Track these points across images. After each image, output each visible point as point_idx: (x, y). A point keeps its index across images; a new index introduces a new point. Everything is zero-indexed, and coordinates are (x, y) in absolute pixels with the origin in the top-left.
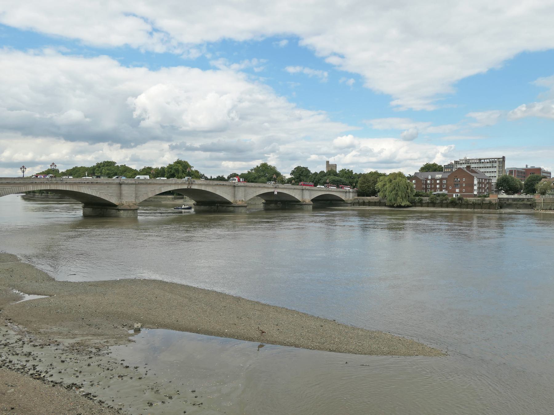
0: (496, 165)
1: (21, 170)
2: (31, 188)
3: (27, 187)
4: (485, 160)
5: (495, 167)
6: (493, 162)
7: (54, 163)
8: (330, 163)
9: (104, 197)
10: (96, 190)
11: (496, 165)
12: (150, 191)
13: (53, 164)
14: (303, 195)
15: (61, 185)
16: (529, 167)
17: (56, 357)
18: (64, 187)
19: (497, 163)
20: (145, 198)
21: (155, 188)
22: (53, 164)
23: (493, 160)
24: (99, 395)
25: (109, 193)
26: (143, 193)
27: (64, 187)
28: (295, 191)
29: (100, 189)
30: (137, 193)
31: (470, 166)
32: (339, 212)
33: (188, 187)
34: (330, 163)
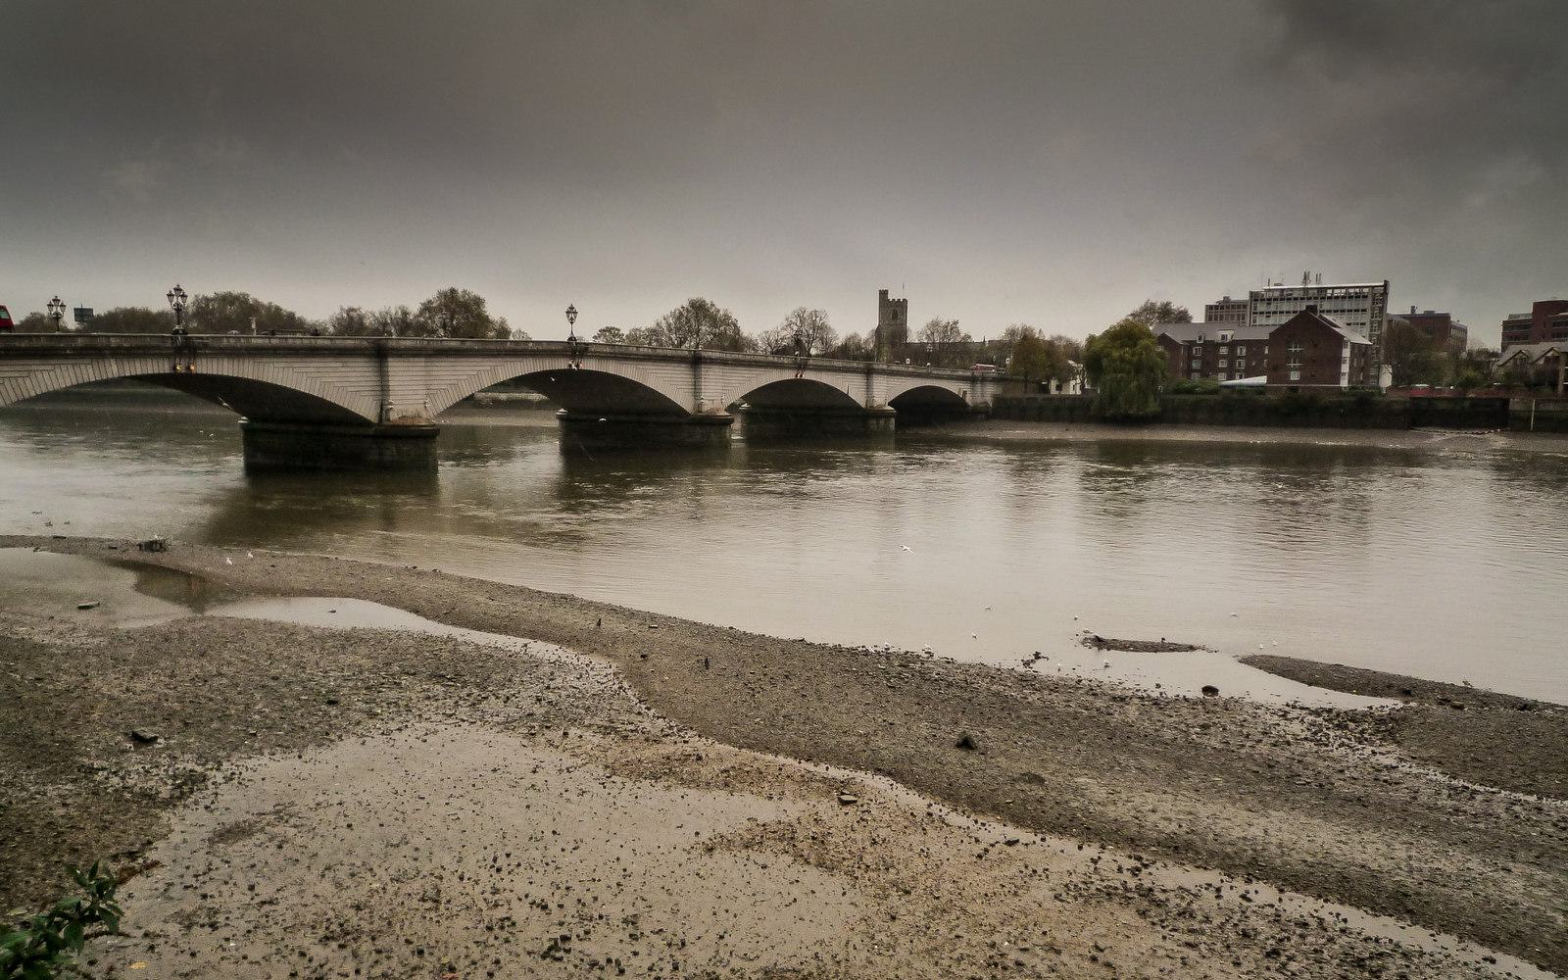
0: (1367, 304)
1: (171, 302)
2: (114, 368)
3: (261, 368)
4: (1336, 291)
5: (1364, 310)
6: (1357, 296)
7: (181, 287)
8: (890, 297)
9: (61, 380)
10: (313, 375)
11: (1367, 304)
12: (476, 373)
13: (56, 300)
14: (869, 387)
15: (204, 361)
16: (1419, 311)
17: (720, 897)
18: (236, 367)
19: (1369, 301)
20: (49, 383)
21: (478, 368)
22: (56, 300)
23: (1357, 290)
24: (713, 893)
25: (347, 384)
26: (447, 382)
27: (236, 367)
28: (849, 376)
29: (321, 370)
30: (431, 382)
31: (1316, 306)
32: (174, 391)
33: (175, 368)
34: (890, 297)
